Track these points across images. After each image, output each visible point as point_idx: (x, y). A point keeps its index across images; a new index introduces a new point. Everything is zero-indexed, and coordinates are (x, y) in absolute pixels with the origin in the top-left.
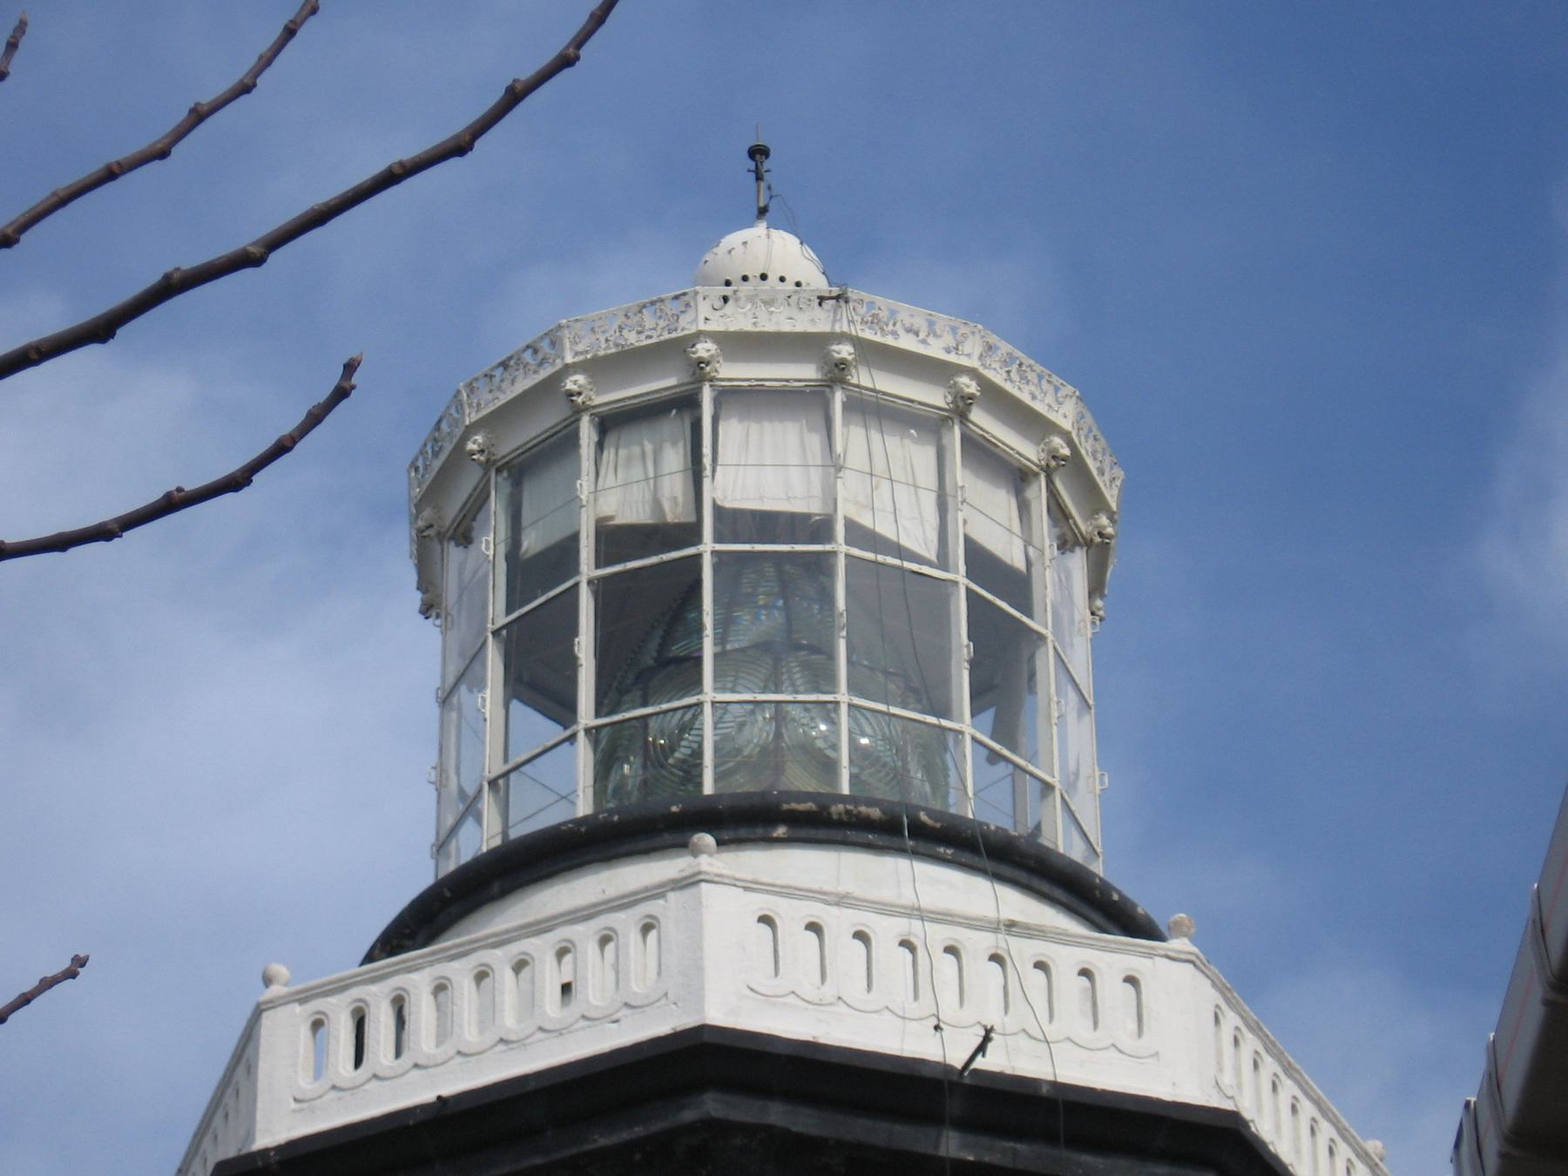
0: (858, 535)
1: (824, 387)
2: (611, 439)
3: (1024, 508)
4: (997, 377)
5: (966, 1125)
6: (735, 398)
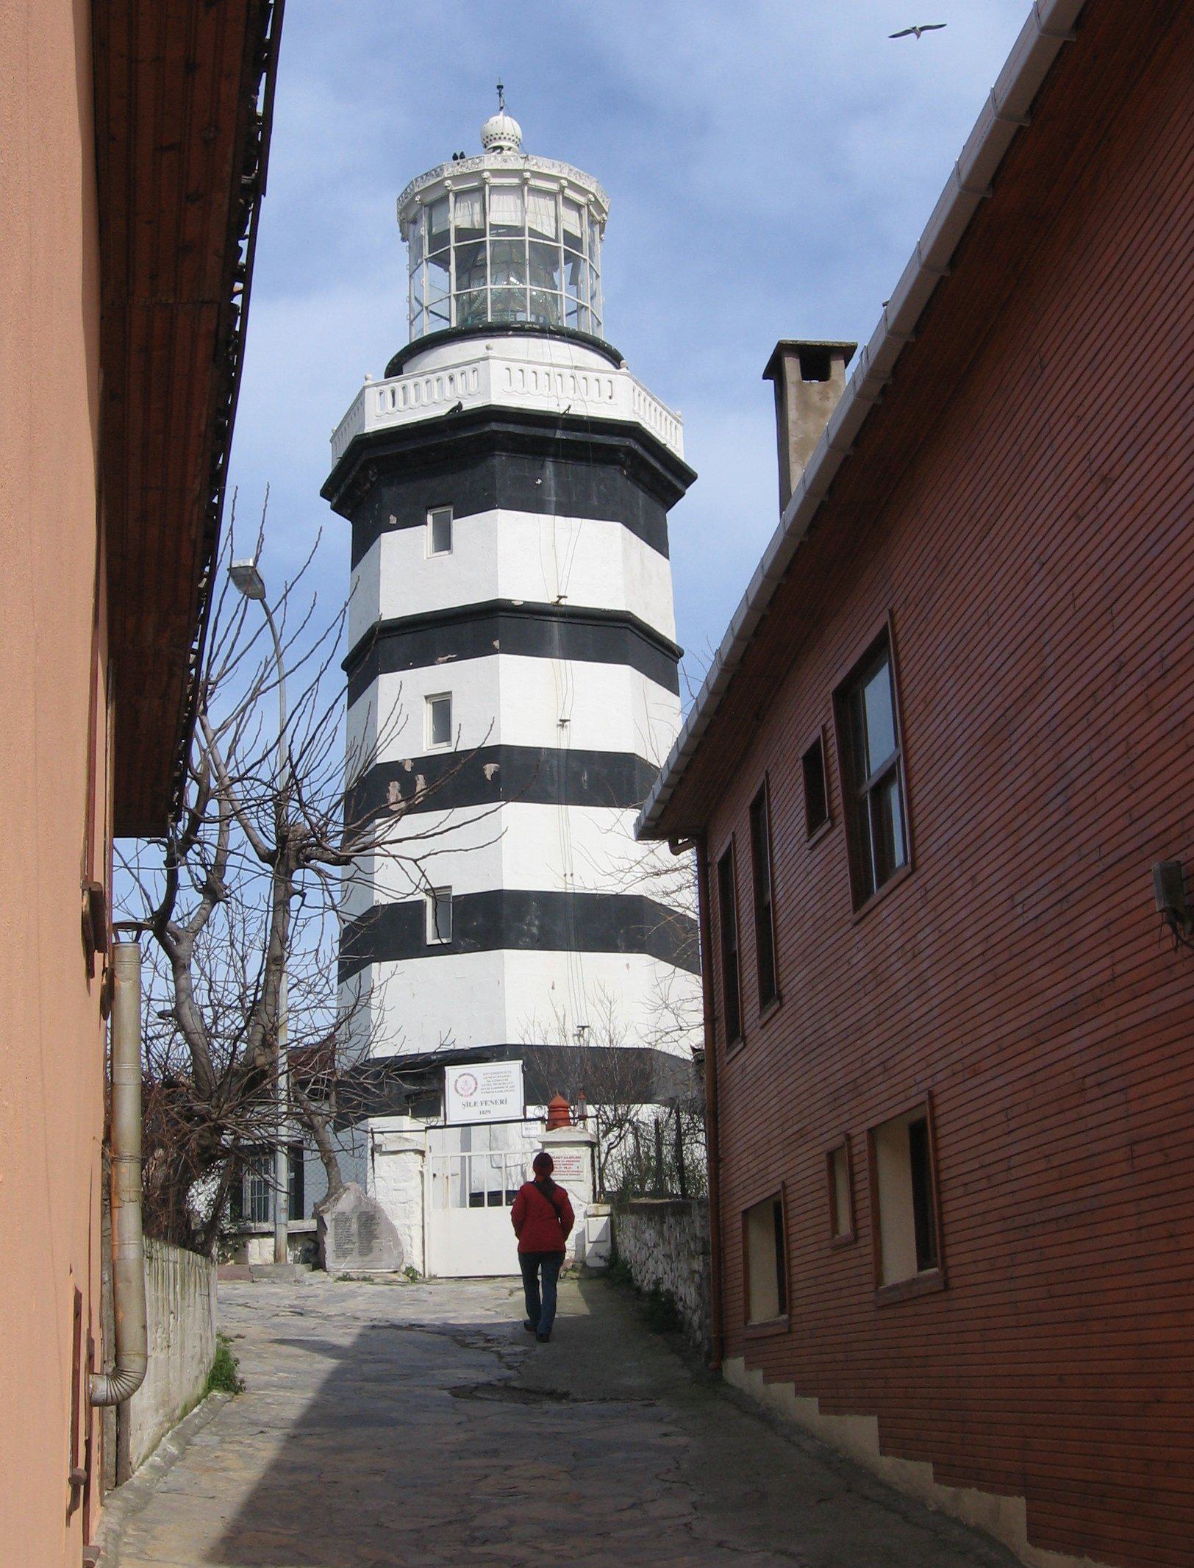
0: (533, 233)
1: (523, 186)
3: (580, 216)
4: (572, 179)
5: (564, 429)
6: (495, 189)
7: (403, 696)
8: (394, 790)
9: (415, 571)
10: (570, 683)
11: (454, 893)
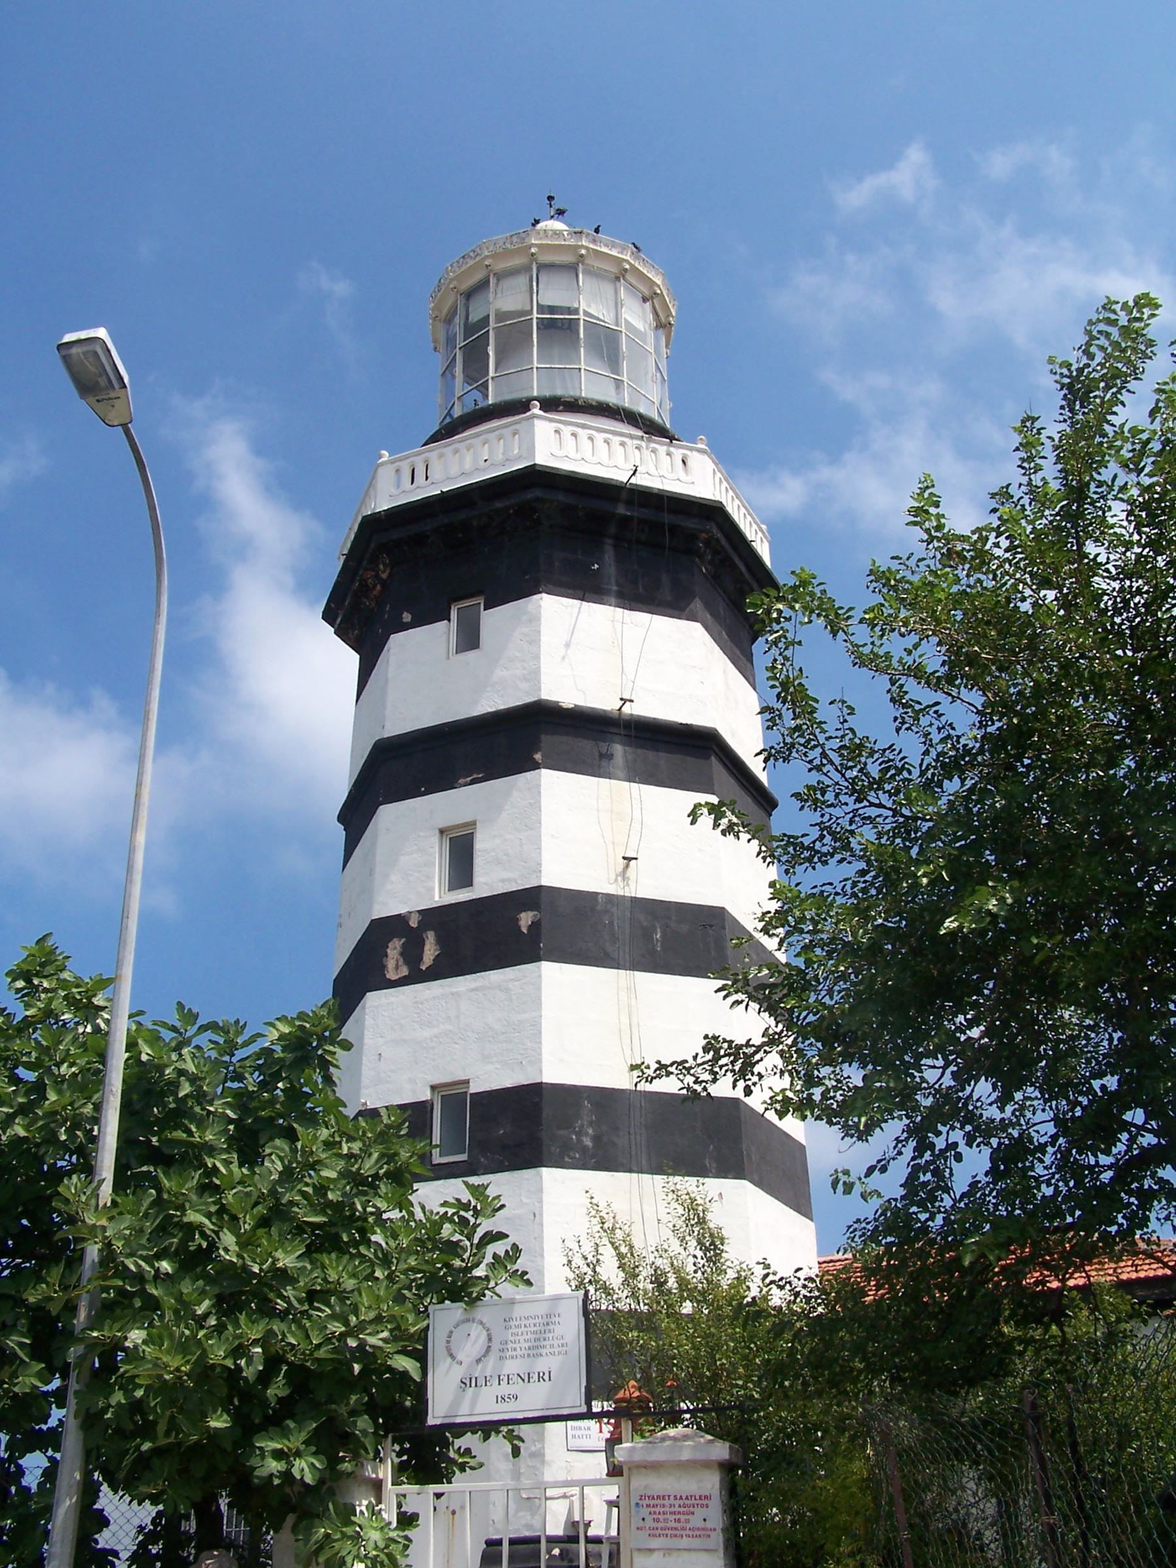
0: (586, 313)
2: (501, 283)
7: (411, 831)
8: (394, 950)
9: (436, 677)
10: (637, 813)
11: (474, 1089)
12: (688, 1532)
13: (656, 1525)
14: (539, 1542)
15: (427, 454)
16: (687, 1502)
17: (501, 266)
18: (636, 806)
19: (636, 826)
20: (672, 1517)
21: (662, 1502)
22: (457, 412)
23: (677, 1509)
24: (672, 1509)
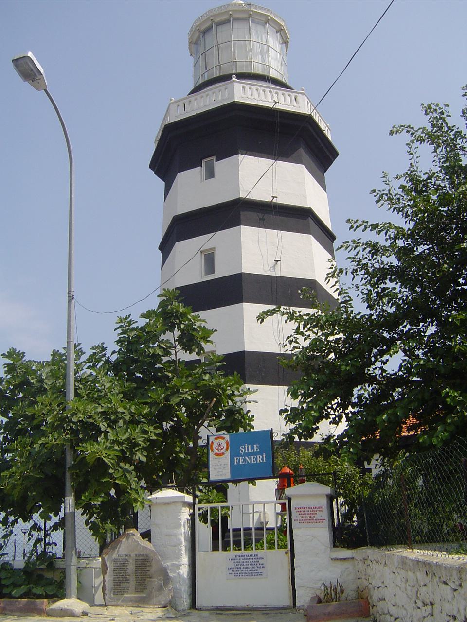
7: (188, 249)
9: (195, 189)
12: (314, 521)
13: (302, 519)
14: (241, 530)
15: (190, 98)
16: (314, 510)
17: (236, 16)
18: (280, 240)
19: (280, 248)
20: (308, 516)
21: (304, 510)
22: (201, 81)
23: (310, 512)
24: (308, 513)
